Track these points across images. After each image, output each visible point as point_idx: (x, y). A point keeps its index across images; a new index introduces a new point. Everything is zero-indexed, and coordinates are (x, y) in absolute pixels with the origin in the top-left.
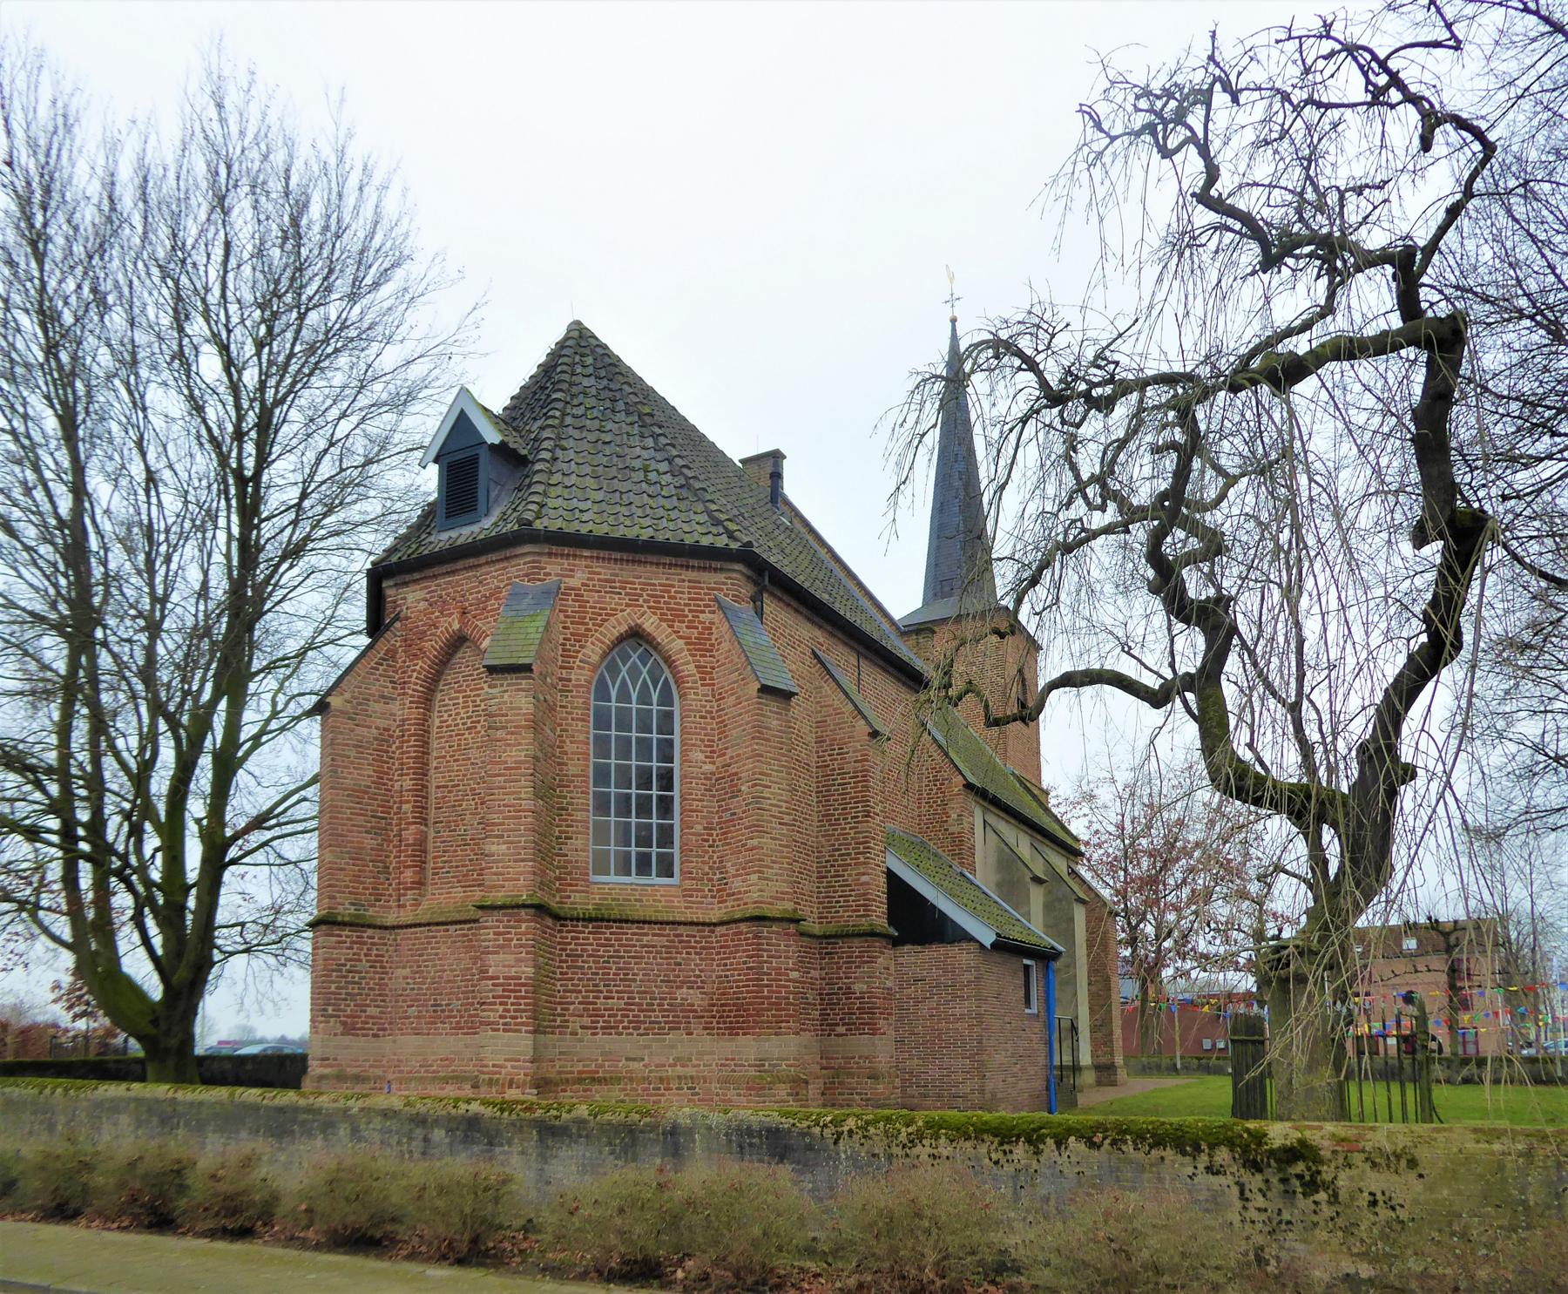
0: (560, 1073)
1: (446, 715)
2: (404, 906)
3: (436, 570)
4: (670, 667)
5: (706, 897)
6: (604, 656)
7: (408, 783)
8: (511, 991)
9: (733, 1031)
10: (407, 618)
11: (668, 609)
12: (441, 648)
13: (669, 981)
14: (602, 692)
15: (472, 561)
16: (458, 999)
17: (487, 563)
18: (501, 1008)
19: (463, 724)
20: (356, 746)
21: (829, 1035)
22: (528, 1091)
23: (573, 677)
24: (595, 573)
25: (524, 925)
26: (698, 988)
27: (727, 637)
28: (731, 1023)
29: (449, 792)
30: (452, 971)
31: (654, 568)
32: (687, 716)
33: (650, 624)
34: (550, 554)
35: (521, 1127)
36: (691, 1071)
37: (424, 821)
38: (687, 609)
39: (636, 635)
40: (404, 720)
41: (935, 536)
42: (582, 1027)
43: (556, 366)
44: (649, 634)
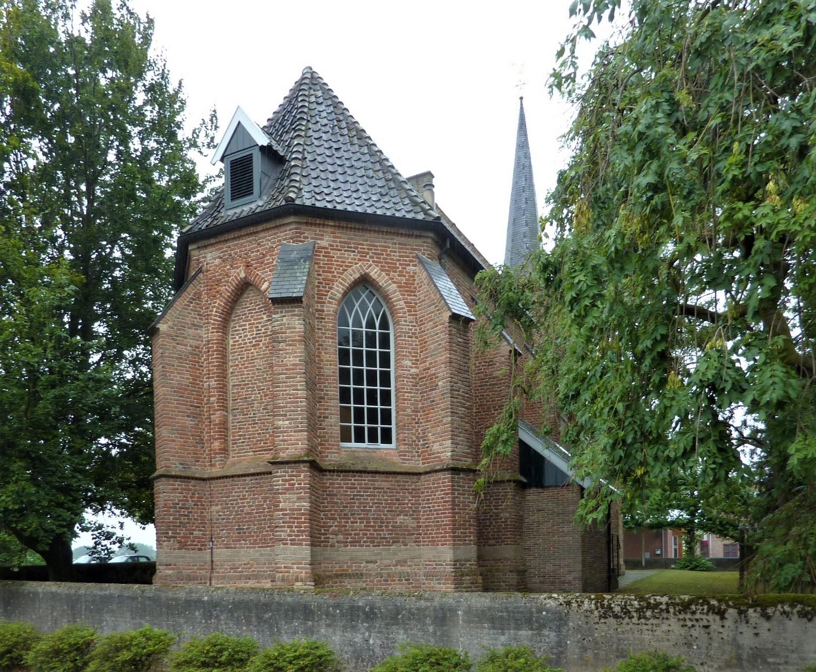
0: (324, 571)
1: (237, 337)
3: (226, 237)
4: (387, 303)
5: (414, 456)
6: (345, 294)
7: (213, 383)
8: (295, 518)
10: (207, 271)
11: (386, 263)
12: (237, 285)
13: (391, 511)
14: (343, 321)
15: (252, 229)
16: (255, 525)
17: (263, 230)
18: (288, 530)
19: (250, 343)
20: (177, 358)
21: (484, 545)
22: (309, 583)
23: (325, 309)
24: (338, 237)
25: (302, 475)
26: (411, 515)
27: (425, 282)
28: (433, 537)
29: (242, 389)
30: (250, 506)
31: (376, 235)
32: (400, 336)
33: (374, 273)
34: (307, 223)
36: (406, 569)
37: (225, 408)
38: (398, 263)
39: (364, 282)
40: (208, 341)
41: (510, 240)
42: (338, 542)
43: (297, 97)
44: (374, 280)
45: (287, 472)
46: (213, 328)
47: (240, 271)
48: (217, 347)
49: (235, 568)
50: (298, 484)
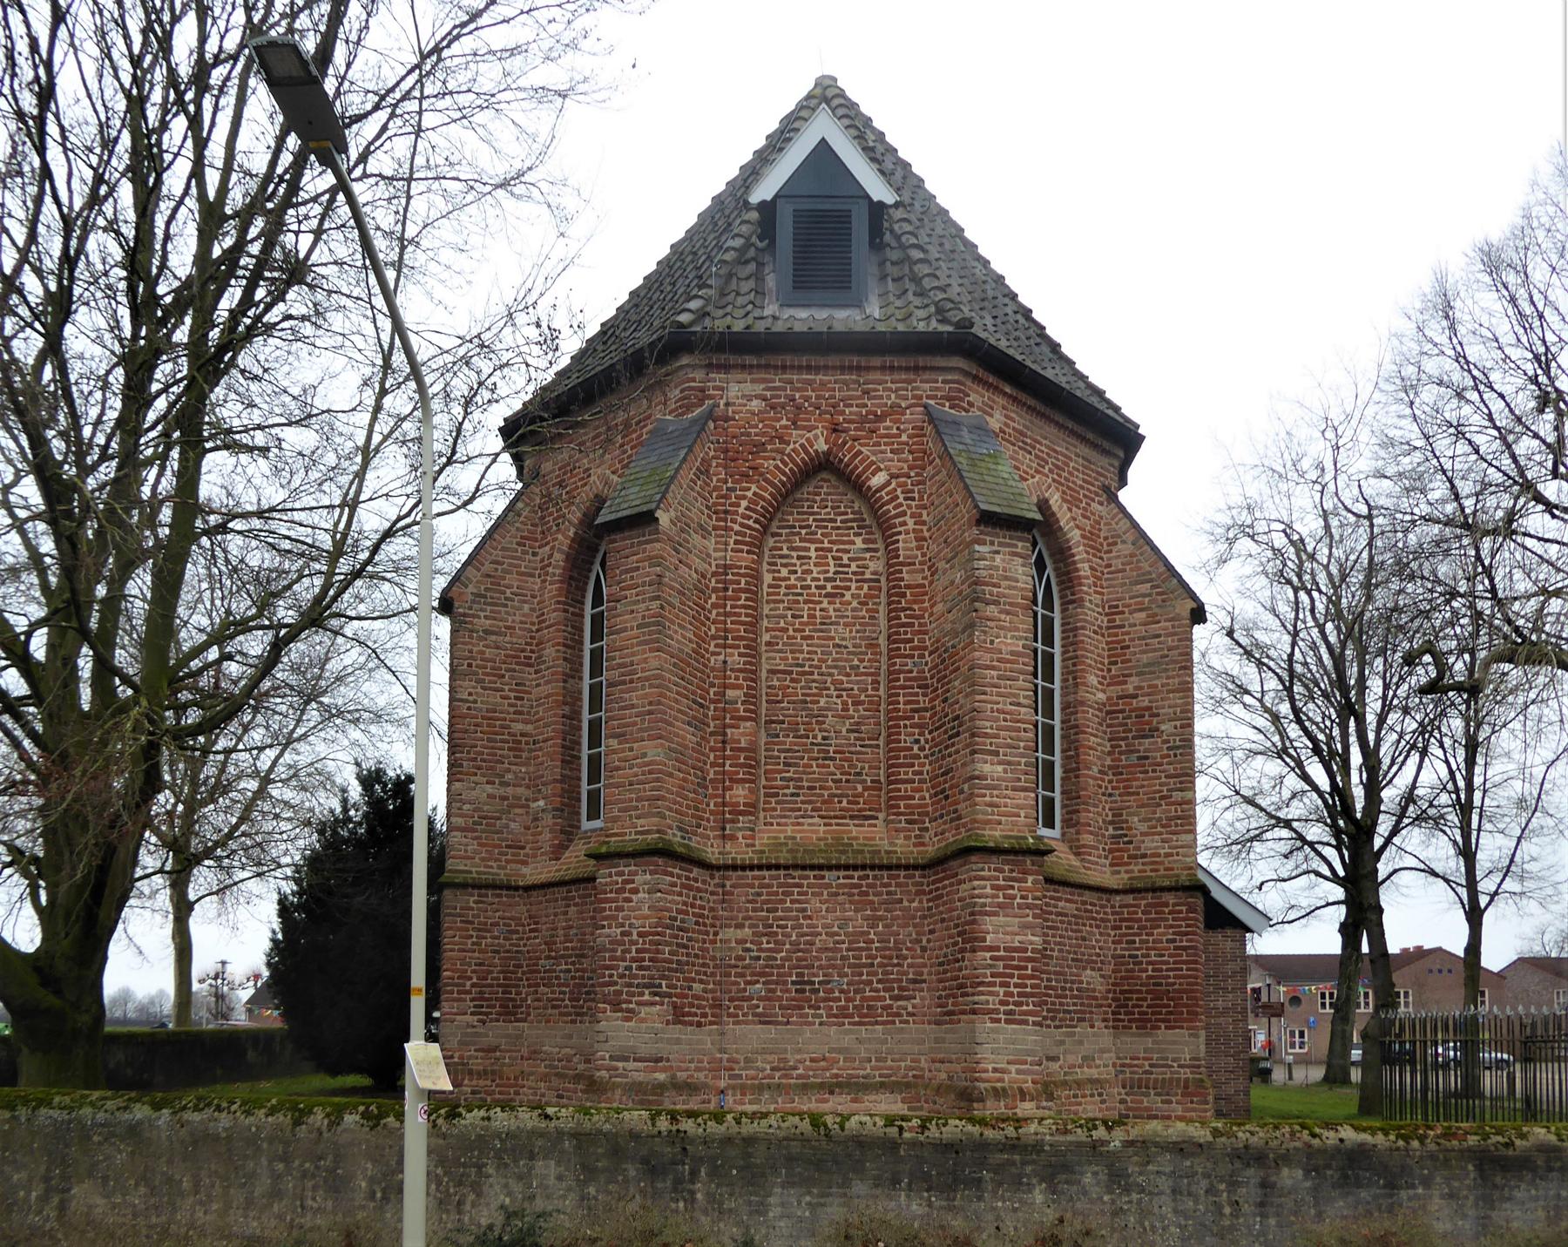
2: (733, 838)
3: (789, 359)
9: (1145, 1024)
10: (727, 419)
17: (883, 368)
18: (1002, 991)
25: (1030, 879)
35: (1446, 1160)
45: (1002, 871)
46: (736, 542)
47: (816, 437)
48: (747, 583)
49: (783, 1067)
50: (1022, 897)
